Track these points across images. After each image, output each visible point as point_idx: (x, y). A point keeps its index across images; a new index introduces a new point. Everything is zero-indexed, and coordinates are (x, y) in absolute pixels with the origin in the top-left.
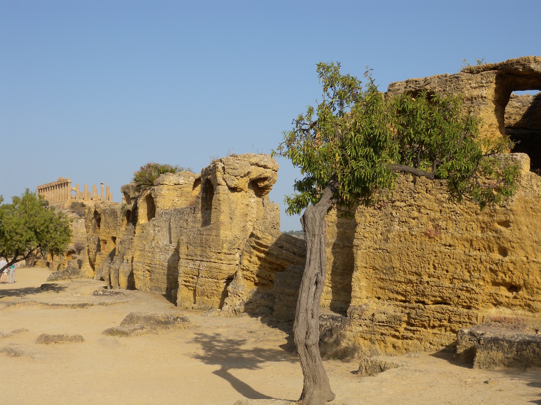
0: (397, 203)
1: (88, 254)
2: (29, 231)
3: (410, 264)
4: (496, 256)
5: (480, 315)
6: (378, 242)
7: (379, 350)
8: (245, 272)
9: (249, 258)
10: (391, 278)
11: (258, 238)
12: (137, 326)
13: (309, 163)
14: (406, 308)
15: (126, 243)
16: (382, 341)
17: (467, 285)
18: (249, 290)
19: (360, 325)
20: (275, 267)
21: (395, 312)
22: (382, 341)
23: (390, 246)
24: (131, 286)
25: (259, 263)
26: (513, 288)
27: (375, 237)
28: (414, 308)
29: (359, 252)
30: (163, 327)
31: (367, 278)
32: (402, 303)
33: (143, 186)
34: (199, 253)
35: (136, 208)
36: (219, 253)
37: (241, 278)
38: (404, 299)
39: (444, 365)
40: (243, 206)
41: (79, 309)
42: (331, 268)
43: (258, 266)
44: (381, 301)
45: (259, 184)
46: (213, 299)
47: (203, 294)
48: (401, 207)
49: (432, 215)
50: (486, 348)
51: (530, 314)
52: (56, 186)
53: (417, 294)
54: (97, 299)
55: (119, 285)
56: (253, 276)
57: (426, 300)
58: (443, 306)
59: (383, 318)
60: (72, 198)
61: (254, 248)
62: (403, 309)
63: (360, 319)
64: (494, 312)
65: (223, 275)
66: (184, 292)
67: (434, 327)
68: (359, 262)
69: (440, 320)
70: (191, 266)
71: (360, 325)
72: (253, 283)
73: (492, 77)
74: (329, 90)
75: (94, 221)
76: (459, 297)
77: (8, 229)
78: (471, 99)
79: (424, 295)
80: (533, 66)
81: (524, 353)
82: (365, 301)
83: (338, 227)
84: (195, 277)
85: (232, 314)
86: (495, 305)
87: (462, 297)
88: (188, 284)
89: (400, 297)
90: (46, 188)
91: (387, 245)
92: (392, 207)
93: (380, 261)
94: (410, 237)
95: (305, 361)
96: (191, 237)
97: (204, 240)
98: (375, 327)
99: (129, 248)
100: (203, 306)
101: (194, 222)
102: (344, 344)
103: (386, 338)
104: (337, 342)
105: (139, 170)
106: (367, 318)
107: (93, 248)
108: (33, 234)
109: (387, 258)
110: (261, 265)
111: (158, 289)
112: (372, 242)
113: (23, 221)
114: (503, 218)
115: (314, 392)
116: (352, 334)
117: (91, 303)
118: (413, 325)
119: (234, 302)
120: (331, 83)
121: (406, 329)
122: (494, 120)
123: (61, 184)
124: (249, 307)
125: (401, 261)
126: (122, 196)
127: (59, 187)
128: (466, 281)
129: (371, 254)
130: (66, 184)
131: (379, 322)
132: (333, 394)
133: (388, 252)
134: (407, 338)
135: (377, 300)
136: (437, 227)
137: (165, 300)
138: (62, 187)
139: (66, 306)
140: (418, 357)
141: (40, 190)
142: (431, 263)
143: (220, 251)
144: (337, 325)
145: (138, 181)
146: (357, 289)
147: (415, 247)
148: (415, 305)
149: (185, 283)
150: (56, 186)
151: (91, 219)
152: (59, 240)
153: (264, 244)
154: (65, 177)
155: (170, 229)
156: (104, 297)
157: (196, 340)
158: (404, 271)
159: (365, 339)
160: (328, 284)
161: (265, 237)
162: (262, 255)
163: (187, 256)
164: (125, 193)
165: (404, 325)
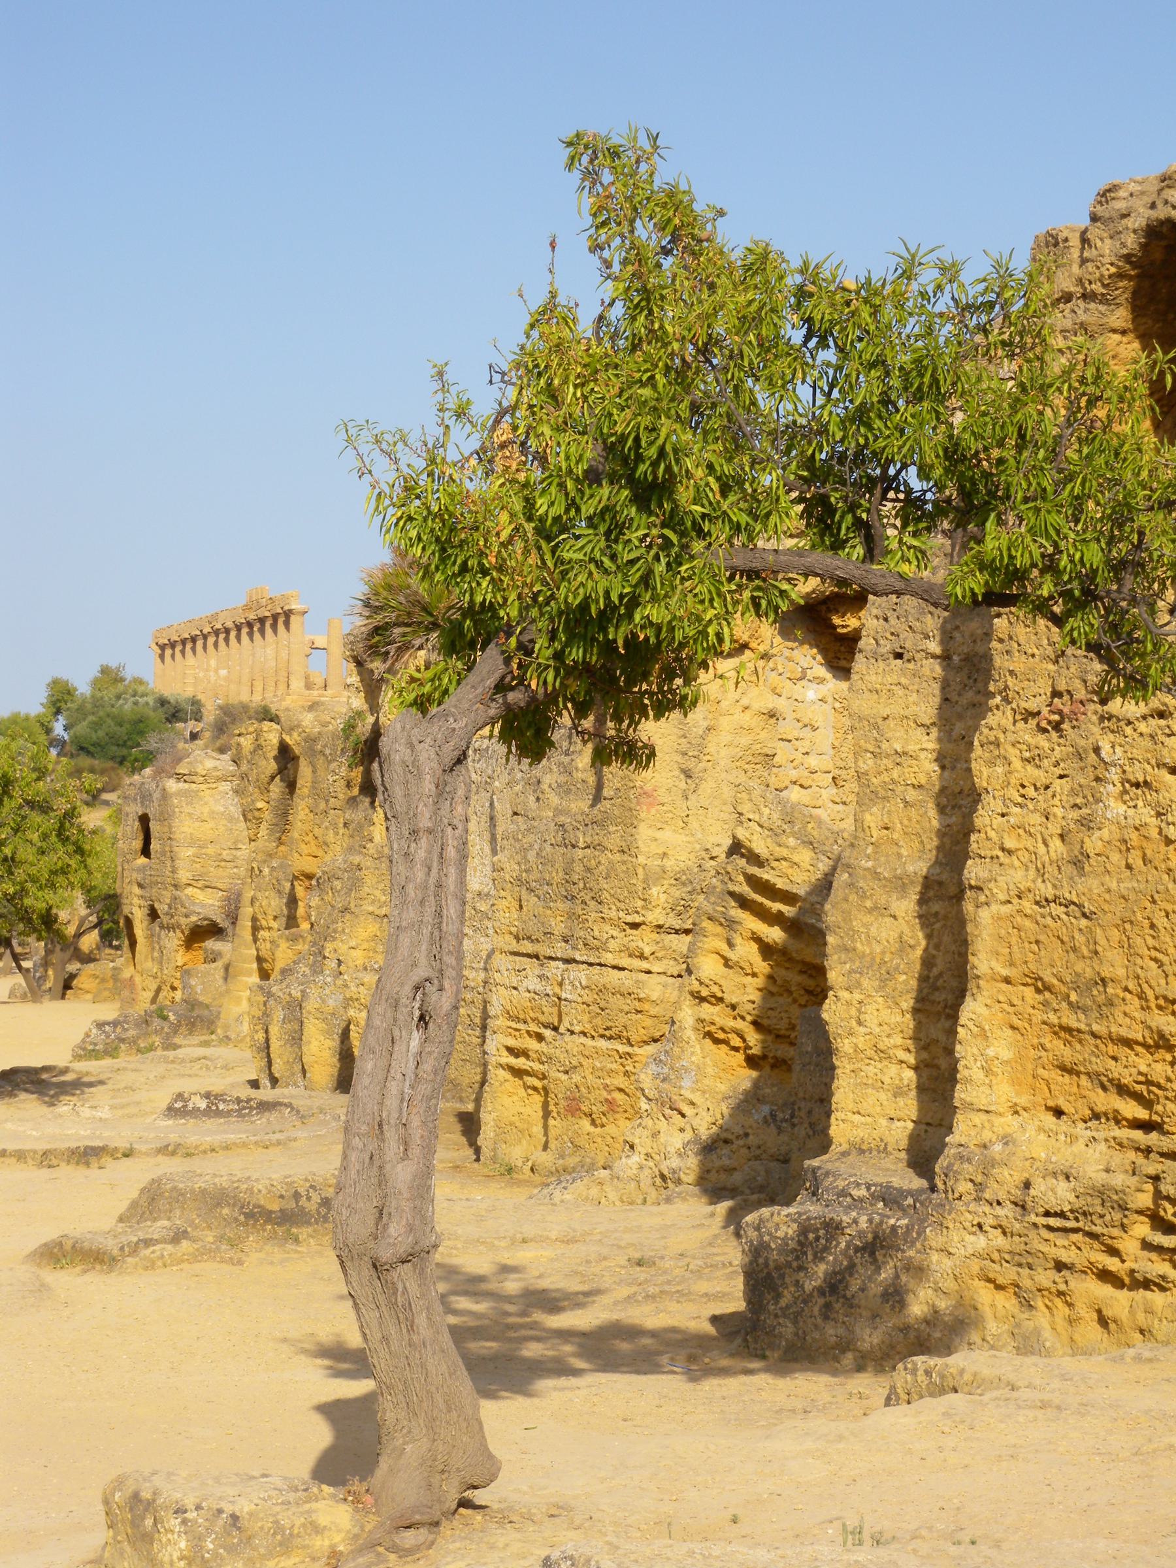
1: (255, 940)
3: (1161, 964)
6: (1051, 870)
7: (1047, 1334)
8: (708, 1011)
9: (724, 947)
10: (1095, 1027)
11: (755, 859)
12: (158, 1228)
14: (1147, 1151)
15: (337, 884)
16: (1061, 1294)
18: (723, 1088)
19: (980, 1226)
21: (1107, 1171)
22: (1061, 1294)
25: (762, 967)
27: (1042, 849)
29: (985, 915)
30: (272, 1237)
31: (1013, 1028)
32: (1138, 1135)
33: (397, 631)
36: (635, 926)
37: (689, 1034)
38: (1142, 1114)
40: (747, 719)
41: (66, 1171)
42: (914, 983)
43: (760, 982)
44: (1063, 1124)
45: (837, 621)
46: (611, 1129)
47: (573, 1108)
48: (1129, 723)
52: (239, 628)
55: (304, 1071)
56: (740, 1024)
59: (1061, 1195)
60: (309, 686)
61: (744, 903)
62: (1140, 1159)
63: (978, 1199)
65: (648, 1022)
66: (507, 1101)
70: (533, 983)
71: (980, 1226)
72: (740, 1057)
75: (277, 788)
82: (1009, 1124)
83: (941, 809)
84: (548, 1033)
85: (653, 1195)
88: (521, 1062)
89: (1132, 1110)
90: (194, 640)
91: (1082, 884)
92: (1102, 718)
93: (1058, 952)
94: (1163, 848)
95: (374, 1324)
96: (531, 856)
97: (578, 868)
98: (1032, 1234)
99: (346, 910)
100: (571, 1161)
101: (564, 790)
103: (1072, 1284)
104: (895, 1296)
106: (1002, 1196)
107: (271, 913)
109: (1080, 939)
110: (770, 977)
112: (1032, 873)
115: (408, 1448)
116: (947, 1263)
117: (123, 1144)
119: (662, 1138)
121: (1146, 1245)
123: (262, 621)
124: (718, 1163)
125: (1131, 953)
127: (251, 634)
129: (1027, 923)
130: (281, 618)
131: (1047, 1214)
132: (491, 1456)
133: (1084, 915)
134: (1146, 1284)
135: (1050, 1119)
138: (262, 632)
139: (20, 1156)
140: (1150, 1360)
141: (168, 647)
143: (638, 919)
144: (894, 1228)
145: (377, 610)
146: (977, 1074)
149: (512, 1060)
150: (239, 628)
151: (264, 778)
152: (33, 870)
153: (780, 884)
154: (277, 587)
156: (210, 1123)
158: (1142, 996)
159: (999, 1287)
160: (902, 1055)
161: (784, 852)
162: (775, 934)
163: (517, 938)
165: (1142, 1229)
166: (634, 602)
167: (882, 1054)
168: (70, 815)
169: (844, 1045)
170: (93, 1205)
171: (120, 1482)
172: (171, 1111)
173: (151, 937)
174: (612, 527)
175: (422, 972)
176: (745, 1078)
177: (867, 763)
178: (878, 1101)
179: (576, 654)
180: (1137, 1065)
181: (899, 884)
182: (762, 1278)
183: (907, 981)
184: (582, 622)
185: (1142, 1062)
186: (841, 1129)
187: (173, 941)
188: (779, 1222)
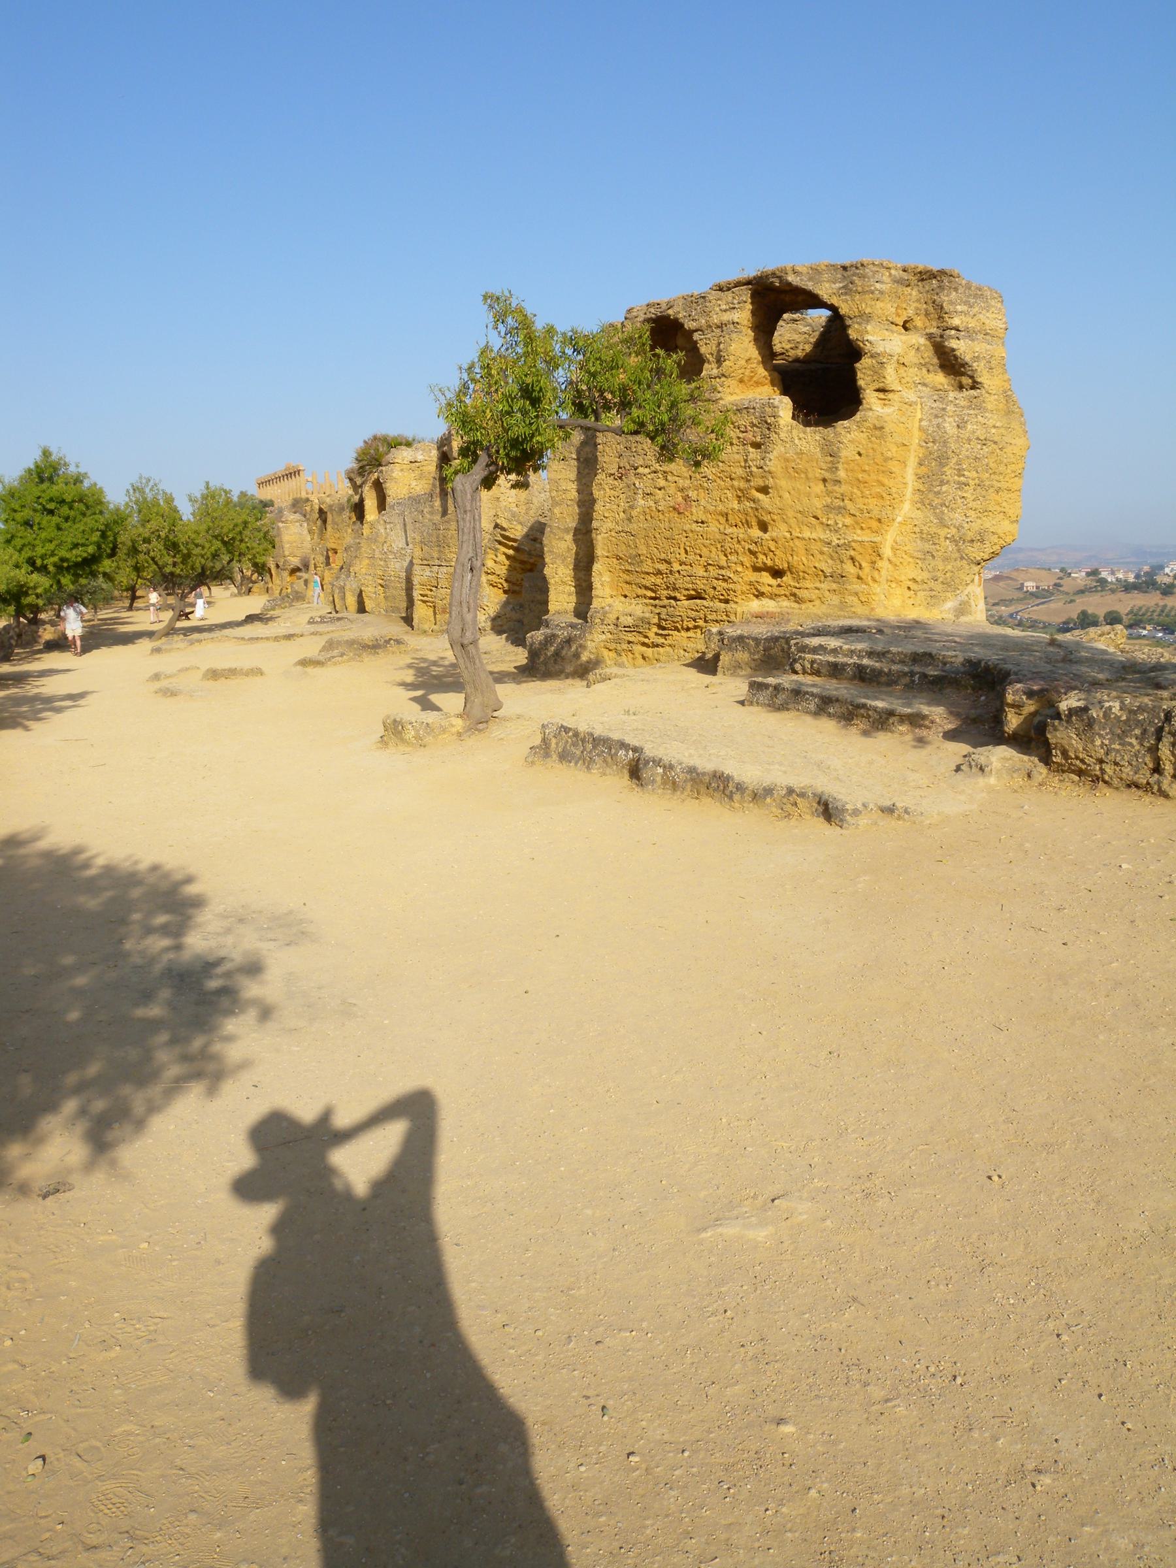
0: (641, 470)
2: (214, 541)
4: (756, 532)
5: (739, 610)
11: (503, 529)
12: (336, 652)
13: (465, 421)
14: (655, 606)
17: (723, 572)
20: (528, 567)
23: (633, 527)
24: (362, 609)
25: (507, 563)
26: (777, 573)
28: (664, 607)
34: (436, 555)
35: (362, 500)
39: (693, 675)
41: (283, 642)
49: (681, 482)
50: (730, 649)
51: (796, 605)
53: (668, 588)
54: (313, 628)
57: (678, 595)
58: (698, 601)
59: (629, 621)
61: (500, 543)
64: (755, 605)
67: (688, 629)
68: (599, 551)
69: (695, 620)
70: (428, 573)
73: (745, 294)
74: (500, 326)
75: (319, 523)
76: (714, 588)
77: (183, 540)
78: (720, 326)
79: (675, 589)
80: (791, 278)
81: (772, 652)
82: (609, 601)
83: (579, 506)
86: (757, 596)
87: (718, 588)
89: (650, 594)
101: (431, 513)
102: (584, 657)
104: (577, 655)
105: (362, 444)
108: (218, 544)
111: (395, 609)
113: (203, 527)
114: (761, 483)
118: (664, 629)
120: (500, 318)
121: (656, 634)
122: (754, 353)
125: (648, 546)
126: (348, 484)
128: (721, 568)
134: (657, 646)
136: (686, 498)
137: (403, 623)
139: (267, 639)
141: (262, 484)
142: (682, 546)
147: (662, 526)
148: (666, 602)
154: (294, 463)
155: (405, 525)
157: (410, 666)
162: (511, 552)
164: (351, 479)
165: (655, 629)
166: (533, 436)
167: (564, 583)
168: (267, 532)
169: (552, 581)
170: (311, 647)
171: (388, 717)
172: (309, 623)
173: (277, 574)
174: (525, 413)
175: (471, 555)
176: (504, 597)
177: (554, 494)
178: (563, 598)
179: (513, 454)
180: (650, 580)
181: (567, 530)
182: (534, 655)
183: (571, 560)
184: (515, 443)
185: (653, 579)
186: (552, 607)
187: (286, 574)
188: (537, 636)
